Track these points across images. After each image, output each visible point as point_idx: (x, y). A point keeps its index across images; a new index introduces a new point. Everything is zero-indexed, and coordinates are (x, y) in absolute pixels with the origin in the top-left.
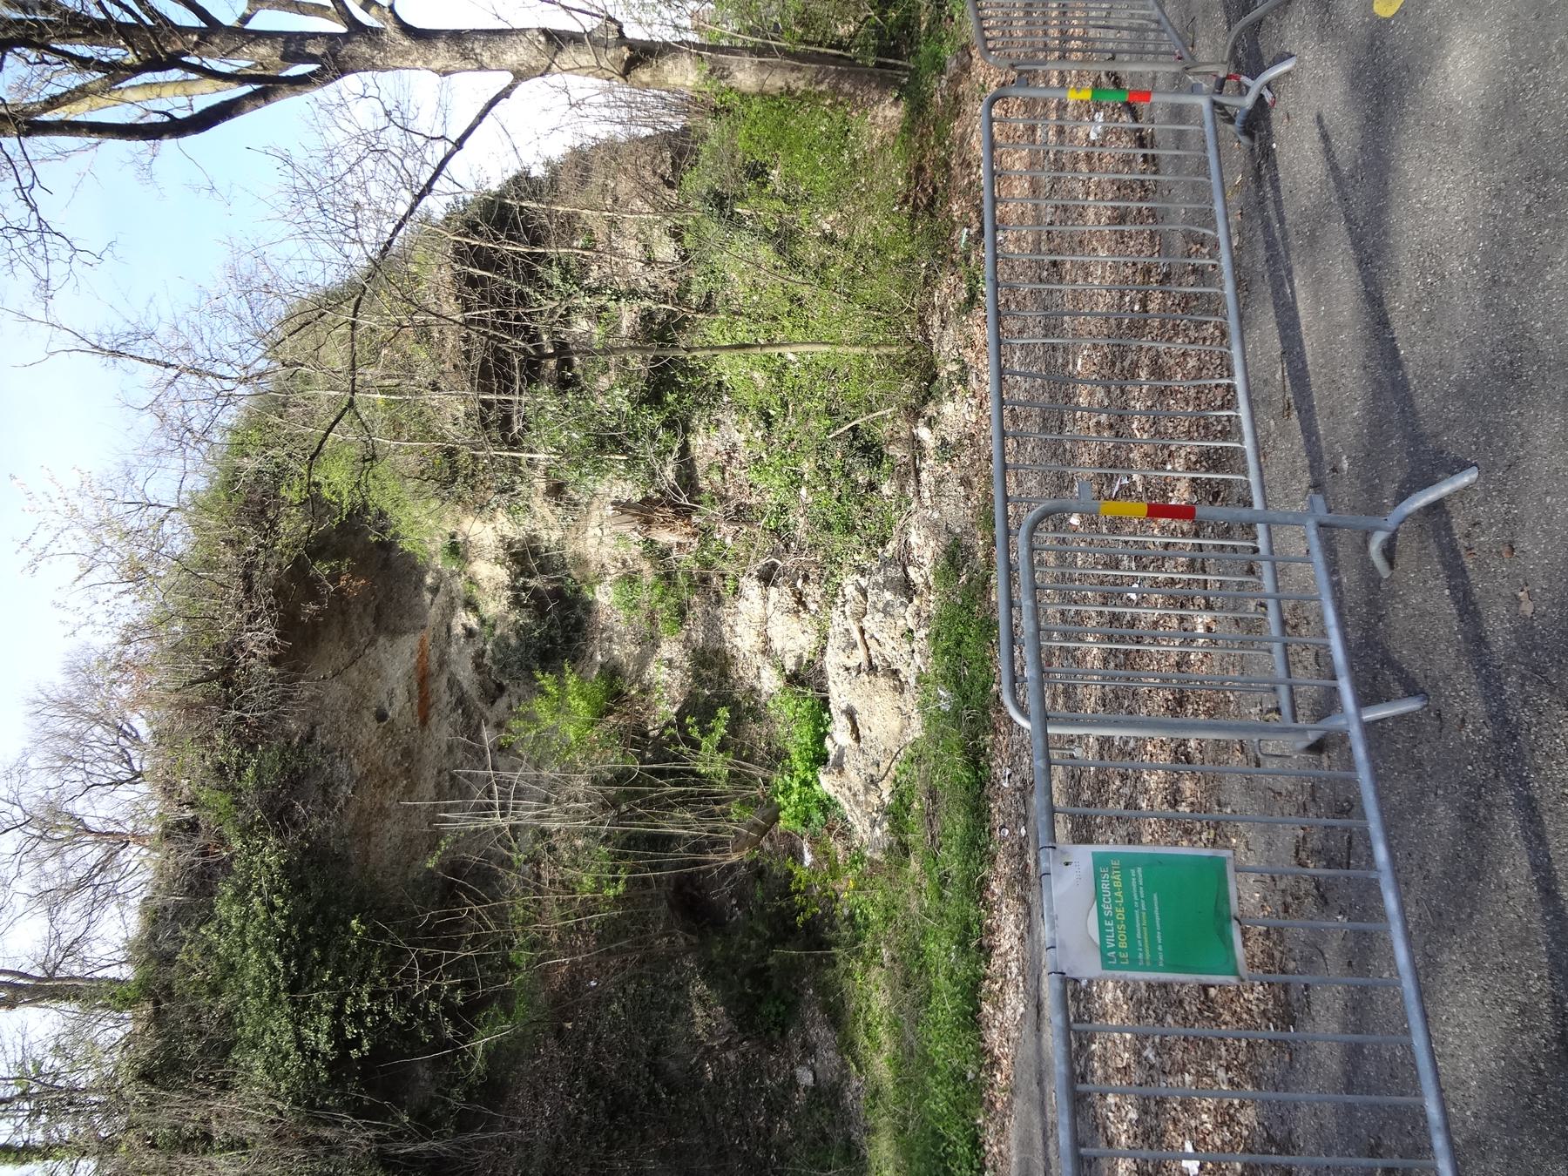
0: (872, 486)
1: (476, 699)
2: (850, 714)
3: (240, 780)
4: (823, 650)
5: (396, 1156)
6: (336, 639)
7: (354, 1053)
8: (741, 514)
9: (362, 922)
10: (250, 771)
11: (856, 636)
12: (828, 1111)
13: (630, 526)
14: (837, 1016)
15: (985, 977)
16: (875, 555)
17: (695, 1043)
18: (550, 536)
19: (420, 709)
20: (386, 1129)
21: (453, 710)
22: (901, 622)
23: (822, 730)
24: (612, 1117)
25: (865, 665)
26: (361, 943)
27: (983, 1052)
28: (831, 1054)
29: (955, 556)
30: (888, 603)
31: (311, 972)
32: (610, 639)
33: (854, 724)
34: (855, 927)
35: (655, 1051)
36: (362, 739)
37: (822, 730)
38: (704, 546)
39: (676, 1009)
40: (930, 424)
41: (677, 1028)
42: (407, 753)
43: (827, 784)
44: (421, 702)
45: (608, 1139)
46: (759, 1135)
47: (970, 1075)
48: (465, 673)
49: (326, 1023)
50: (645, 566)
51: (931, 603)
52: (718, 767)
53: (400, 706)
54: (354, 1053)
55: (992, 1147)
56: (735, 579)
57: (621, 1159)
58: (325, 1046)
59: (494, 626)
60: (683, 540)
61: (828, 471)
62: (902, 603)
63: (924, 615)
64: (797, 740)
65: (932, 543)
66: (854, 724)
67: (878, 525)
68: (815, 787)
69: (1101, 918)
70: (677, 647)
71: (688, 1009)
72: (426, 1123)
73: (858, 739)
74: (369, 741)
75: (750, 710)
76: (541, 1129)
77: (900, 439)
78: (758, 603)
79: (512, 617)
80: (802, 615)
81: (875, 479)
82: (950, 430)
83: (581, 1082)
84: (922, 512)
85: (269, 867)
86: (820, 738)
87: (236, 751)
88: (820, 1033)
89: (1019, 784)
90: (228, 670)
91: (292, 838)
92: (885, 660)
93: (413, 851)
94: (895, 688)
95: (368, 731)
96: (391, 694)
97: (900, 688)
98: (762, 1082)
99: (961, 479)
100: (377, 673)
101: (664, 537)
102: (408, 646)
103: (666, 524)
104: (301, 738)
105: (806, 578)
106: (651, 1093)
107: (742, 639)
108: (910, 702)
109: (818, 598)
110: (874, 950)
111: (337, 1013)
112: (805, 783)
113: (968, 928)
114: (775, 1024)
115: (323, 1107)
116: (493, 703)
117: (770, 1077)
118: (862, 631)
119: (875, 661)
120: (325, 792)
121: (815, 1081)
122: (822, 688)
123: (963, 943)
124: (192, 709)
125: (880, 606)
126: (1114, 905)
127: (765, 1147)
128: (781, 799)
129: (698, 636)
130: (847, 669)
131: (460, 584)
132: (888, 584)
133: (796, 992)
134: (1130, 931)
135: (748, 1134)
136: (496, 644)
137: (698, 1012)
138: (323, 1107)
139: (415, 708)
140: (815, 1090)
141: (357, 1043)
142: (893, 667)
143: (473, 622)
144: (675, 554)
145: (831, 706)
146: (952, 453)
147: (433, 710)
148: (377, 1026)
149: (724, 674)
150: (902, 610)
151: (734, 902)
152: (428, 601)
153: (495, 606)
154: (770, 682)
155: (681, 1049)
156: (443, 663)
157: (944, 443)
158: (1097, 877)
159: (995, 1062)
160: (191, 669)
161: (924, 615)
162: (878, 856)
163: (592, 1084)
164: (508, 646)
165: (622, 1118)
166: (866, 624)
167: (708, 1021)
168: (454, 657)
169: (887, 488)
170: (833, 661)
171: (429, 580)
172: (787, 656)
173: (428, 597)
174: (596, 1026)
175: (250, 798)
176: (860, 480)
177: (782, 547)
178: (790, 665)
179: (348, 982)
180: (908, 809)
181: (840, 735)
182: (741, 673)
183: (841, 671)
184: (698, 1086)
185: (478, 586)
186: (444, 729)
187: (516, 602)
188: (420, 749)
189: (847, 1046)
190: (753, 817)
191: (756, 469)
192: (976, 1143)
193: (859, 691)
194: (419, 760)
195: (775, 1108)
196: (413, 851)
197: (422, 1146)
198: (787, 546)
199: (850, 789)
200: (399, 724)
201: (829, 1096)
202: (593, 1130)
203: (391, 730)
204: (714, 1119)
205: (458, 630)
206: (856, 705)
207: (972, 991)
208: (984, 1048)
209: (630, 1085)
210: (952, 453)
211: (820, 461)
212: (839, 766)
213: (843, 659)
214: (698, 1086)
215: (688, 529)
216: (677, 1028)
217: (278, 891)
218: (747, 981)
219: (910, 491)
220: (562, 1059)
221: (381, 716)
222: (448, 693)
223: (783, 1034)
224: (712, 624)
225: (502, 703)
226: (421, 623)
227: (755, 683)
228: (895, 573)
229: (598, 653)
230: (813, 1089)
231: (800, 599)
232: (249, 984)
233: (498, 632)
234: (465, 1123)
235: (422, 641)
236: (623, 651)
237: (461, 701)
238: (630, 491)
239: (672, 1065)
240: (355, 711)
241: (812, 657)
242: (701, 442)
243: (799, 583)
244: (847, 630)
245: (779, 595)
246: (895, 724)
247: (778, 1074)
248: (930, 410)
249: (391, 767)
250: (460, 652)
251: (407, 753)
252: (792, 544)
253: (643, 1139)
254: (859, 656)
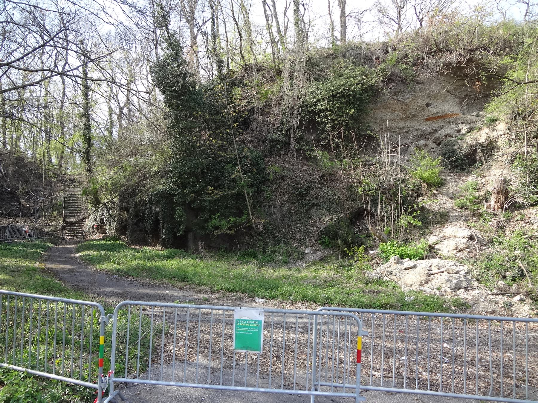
0: (504, 277)
1: (435, 136)
2: (414, 267)
3: (402, 64)
4: (441, 258)
5: (290, 133)
6: (457, 84)
7: (317, 117)
8: (501, 228)
9: (354, 112)
10: (405, 66)
11: (441, 270)
12: (296, 257)
13: (496, 186)
14: (324, 260)
15: (316, 304)
16: (473, 277)
17: (320, 217)
18: (498, 154)
19: (431, 118)
20: (297, 129)
21: (432, 129)
22: (444, 285)
23: (412, 257)
24: (299, 194)
25: (431, 272)
26: (348, 114)
27: (296, 302)
28: (313, 258)
29: (463, 306)
30: (452, 281)
31: (338, 100)
32: (455, 182)
33: (410, 268)
34: (348, 266)
35: (318, 205)
36: (419, 100)
37: (412, 257)
38: (489, 214)
39: (329, 211)
40: (522, 300)
41: (324, 212)
42: (415, 116)
43: (392, 258)
44: (434, 117)
45: (294, 193)
46: (294, 236)
47: (290, 297)
48: (442, 133)
49: (324, 107)
50: (482, 193)
51: (448, 297)
52: (403, 222)
53: (432, 111)
54: (317, 117)
55: (271, 302)
56: (475, 226)
57: (288, 197)
58: (318, 108)
59: (461, 139)
60: (492, 206)
61: (514, 261)
62: (451, 286)
63: (444, 294)
64: (410, 249)
65: (470, 298)
66: (410, 268)
67: (487, 279)
68: (393, 255)
69: (247, 320)
70: (450, 206)
71: (330, 214)
72: (299, 140)
73: (405, 269)
74: (418, 103)
75: (424, 232)
76: (297, 173)
77: (519, 288)
78: (461, 235)
79: (465, 145)
80: (456, 251)
81: (508, 278)
82: (517, 307)
83: (309, 184)
84: (485, 295)
85: (371, 80)
86: (410, 257)
87: (412, 60)
88: (319, 255)
89: (370, 319)
90: (441, 51)
91: (381, 85)
92: (432, 279)
93: (381, 123)
94: (421, 282)
95: (421, 102)
96: (436, 107)
97: (421, 284)
98: (308, 237)
99: (495, 310)
100: (444, 101)
101: (493, 200)
102: (456, 110)
103: (498, 200)
104: (418, 80)
105: (470, 252)
106: (306, 205)
107: (450, 230)
108: (416, 288)
109: (461, 256)
110: (339, 272)
111: (326, 110)
112: (394, 251)
113: (331, 300)
114: (322, 241)
115: (302, 111)
116: (434, 142)
117: (309, 240)
118: (443, 272)
119: (432, 276)
120: (399, 92)
121: (306, 253)
122: (427, 257)
123: (327, 298)
124: (428, 41)
125: (451, 278)
126: (250, 324)
127: (290, 238)
128: (389, 243)
129: (454, 213)
130: (431, 266)
131: (479, 125)
132: (459, 281)
133: (332, 248)
134: (244, 326)
135: (294, 233)
136: (454, 141)
137: (328, 218)
138: (302, 111)
139: (431, 116)
140: (303, 253)
141: (319, 117)
142: (429, 282)
143: (464, 132)
144: (486, 204)
145: (420, 260)
146: (507, 308)
147: (431, 122)
148: (324, 122)
149: (438, 223)
150: (449, 286)
151: (360, 228)
152: (473, 114)
153: (469, 140)
154: (432, 239)
155: (318, 213)
156: (449, 123)
157: (512, 305)
158: (256, 321)
159: (292, 305)
160: (440, 38)
161: (444, 294)
162: (366, 275)
163: (308, 187)
164: (454, 145)
165: (299, 197)
166: (446, 273)
167: (326, 221)
168: (450, 127)
169: (501, 283)
170: (435, 262)
171: (481, 113)
172: (440, 245)
173: (475, 113)
174: (325, 187)
175: (396, 69)
176: (508, 273)
177: (485, 243)
178: (437, 247)
179: (336, 112)
180: (380, 285)
181: (408, 263)
182: (438, 229)
183: (430, 264)
184: (308, 218)
185: (478, 132)
186: (424, 127)
187: (471, 146)
188: (417, 120)
189: (314, 263)
190: (384, 234)
191: (520, 233)
192: (273, 298)
193: (422, 270)
194: (412, 120)
195: (300, 241)
196: (381, 123)
197: (292, 139)
198: (485, 245)
199: (390, 266)
200: (425, 111)
201: (301, 257)
202: (296, 188)
203: (423, 109)
204: (299, 223)
205: (460, 127)
206: (417, 269)
207: (313, 300)
208: (297, 302)
209: (308, 198)
210: (507, 308)
211: (519, 258)
212: (397, 263)
213: (434, 265)
214: (308, 218)
215: (496, 208)
216: (324, 212)
217: (363, 85)
218: (333, 233)
219: (495, 291)
220: (316, 177)
221: (428, 105)
222: (438, 126)
223: (320, 244)
224: (457, 218)
225: (434, 145)
226: (466, 113)
227: (434, 234)
228: (464, 284)
229: (451, 178)
230: (304, 253)
231: (462, 250)
232: (335, 82)
233: (459, 141)
234: (298, 151)
235: (457, 114)
236: (451, 187)
237: (435, 131)
238: (515, 185)
239: (314, 210)
240: (429, 96)
241: (440, 254)
242: (534, 211)
243: (468, 250)
244: (445, 267)
245: (463, 243)
246: (409, 282)
247: (309, 242)
248: (528, 300)
249: (409, 111)
250: (452, 129)
251: (415, 116)
252: (486, 247)
253: (294, 203)
254: (435, 270)
